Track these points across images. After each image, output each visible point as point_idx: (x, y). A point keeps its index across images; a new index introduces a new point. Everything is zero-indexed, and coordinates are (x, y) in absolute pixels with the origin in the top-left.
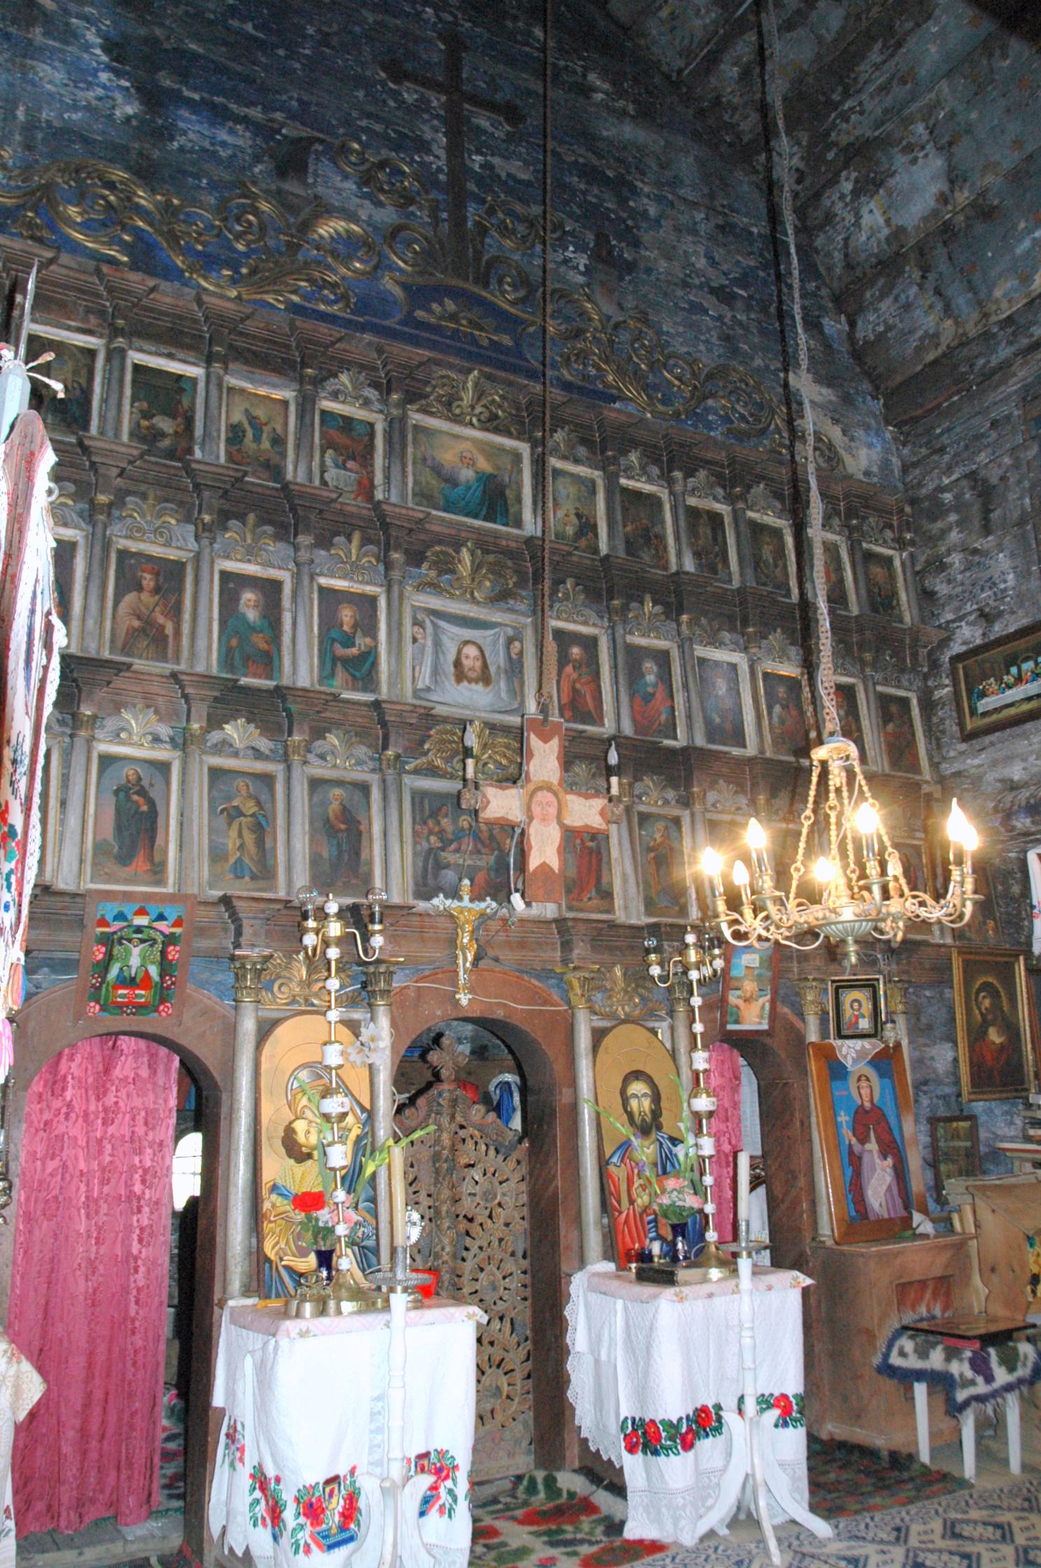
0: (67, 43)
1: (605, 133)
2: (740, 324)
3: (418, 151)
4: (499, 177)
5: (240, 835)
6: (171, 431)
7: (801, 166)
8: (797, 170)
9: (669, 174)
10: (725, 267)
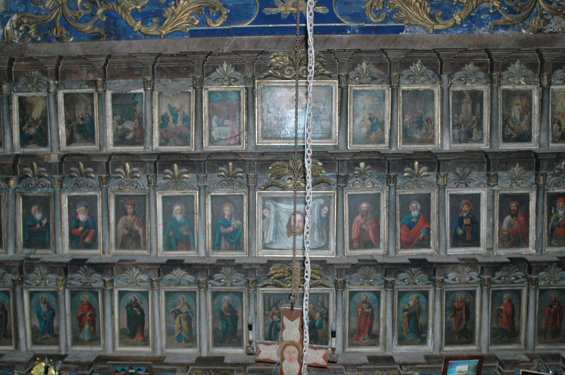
5: (180, 322)
6: (132, 128)
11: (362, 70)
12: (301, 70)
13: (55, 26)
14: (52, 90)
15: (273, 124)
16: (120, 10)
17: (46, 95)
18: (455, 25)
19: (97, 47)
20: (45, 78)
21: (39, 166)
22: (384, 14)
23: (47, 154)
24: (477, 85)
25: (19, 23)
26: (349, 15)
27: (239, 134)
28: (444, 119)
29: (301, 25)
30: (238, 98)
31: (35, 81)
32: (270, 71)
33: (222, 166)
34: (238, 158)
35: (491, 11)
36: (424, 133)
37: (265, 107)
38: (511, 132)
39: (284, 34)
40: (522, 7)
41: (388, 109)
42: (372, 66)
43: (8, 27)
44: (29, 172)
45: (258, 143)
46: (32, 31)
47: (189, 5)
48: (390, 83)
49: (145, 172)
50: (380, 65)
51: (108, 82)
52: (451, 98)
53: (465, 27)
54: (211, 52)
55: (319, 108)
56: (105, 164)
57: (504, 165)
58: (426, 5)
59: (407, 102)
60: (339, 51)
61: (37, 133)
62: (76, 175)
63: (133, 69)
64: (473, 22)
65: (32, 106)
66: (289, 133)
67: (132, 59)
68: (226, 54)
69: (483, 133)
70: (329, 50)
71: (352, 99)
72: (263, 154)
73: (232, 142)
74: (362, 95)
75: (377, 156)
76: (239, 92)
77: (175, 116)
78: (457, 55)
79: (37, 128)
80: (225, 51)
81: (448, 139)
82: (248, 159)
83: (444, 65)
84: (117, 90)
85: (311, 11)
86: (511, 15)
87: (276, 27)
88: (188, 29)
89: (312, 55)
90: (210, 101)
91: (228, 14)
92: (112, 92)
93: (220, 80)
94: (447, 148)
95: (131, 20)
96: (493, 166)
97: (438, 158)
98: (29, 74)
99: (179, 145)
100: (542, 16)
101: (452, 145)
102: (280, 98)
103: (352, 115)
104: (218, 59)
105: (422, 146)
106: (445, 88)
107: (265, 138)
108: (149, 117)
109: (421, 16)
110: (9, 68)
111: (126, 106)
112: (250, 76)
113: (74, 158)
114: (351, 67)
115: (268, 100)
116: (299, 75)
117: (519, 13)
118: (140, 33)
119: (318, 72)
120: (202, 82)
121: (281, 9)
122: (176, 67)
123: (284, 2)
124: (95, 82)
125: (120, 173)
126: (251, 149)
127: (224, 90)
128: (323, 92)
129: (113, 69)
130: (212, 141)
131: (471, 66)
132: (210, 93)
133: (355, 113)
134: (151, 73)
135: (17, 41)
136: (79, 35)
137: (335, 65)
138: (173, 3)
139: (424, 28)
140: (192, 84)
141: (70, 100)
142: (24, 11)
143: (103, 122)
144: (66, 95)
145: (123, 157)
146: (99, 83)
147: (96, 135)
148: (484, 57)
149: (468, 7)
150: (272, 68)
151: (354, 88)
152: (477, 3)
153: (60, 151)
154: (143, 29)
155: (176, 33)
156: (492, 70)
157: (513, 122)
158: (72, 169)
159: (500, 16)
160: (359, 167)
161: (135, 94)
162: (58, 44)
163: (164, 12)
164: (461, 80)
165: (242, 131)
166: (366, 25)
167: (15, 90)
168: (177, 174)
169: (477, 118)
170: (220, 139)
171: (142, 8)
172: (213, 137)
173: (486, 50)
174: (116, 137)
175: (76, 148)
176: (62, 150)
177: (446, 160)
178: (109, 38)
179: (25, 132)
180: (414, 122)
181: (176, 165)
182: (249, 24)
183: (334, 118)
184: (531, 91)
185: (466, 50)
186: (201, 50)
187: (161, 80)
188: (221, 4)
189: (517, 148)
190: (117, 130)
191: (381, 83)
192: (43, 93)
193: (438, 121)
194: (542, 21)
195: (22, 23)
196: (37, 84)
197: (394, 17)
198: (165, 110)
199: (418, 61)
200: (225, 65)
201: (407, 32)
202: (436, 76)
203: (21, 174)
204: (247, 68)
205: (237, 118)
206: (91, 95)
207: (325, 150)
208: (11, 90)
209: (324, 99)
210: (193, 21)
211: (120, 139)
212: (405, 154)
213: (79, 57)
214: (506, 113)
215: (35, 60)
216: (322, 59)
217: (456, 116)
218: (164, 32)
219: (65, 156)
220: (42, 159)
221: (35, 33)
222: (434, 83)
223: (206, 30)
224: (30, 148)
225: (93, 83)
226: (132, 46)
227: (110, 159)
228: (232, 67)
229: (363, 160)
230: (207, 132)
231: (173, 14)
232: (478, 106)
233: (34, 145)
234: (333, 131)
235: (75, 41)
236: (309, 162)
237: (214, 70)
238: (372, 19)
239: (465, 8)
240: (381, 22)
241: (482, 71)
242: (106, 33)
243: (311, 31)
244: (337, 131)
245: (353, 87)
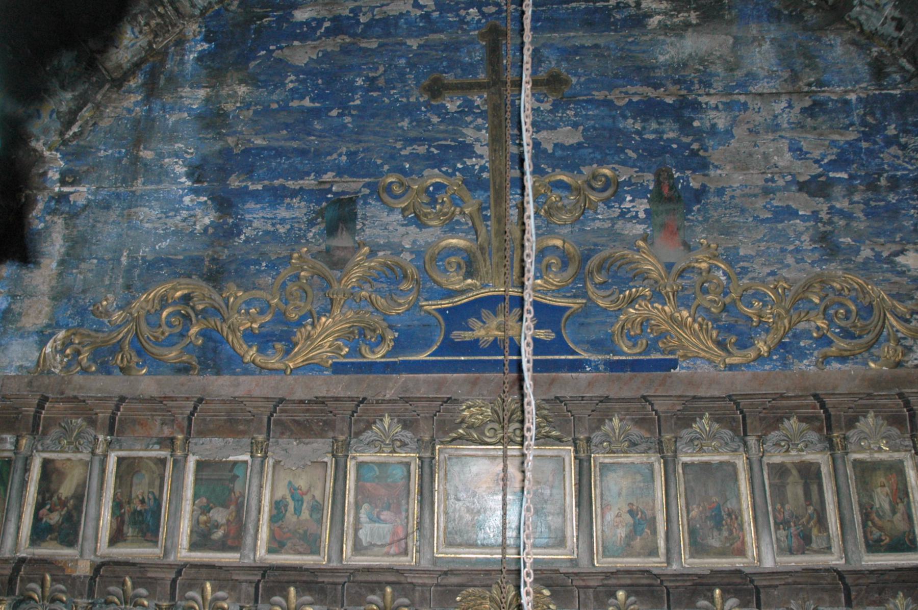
0: (160, 182)
1: (662, 59)
2: (841, 213)
3: (460, 159)
4: (545, 151)
6: (224, 521)
7: (897, 14)
8: (893, 19)
9: (739, 74)
10: (816, 154)
11: (613, 430)
12: (511, 430)
13: (122, 349)
14: (99, 451)
15: (464, 521)
16: (225, 329)
17: (88, 459)
18: (759, 356)
19: (182, 385)
20: (91, 431)
21: (54, 580)
22: (644, 342)
23: (72, 561)
24: (808, 453)
25: (66, 343)
26: (588, 342)
27: (406, 537)
28: (759, 513)
29: (510, 358)
30: (405, 473)
31: (75, 434)
32: (461, 431)
33: (373, 592)
34: (402, 579)
35: (815, 335)
36: (726, 538)
37: (451, 491)
38: (878, 534)
39: (484, 372)
40: (863, 328)
41: (660, 495)
42: (629, 423)
43: (48, 349)
44: (34, 591)
45: (438, 553)
46: (84, 357)
47: (334, 324)
48: (661, 451)
49: (238, 600)
50: (642, 422)
51: (193, 441)
52: (766, 476)
53: (776, 360)
54: (364, 399)
55: (542, 494)
56: (169, 582)
57: (877, 595)
58: (710, 326)
59: (692, 484)
60: (573, 398)
61: (62, 523)
62: (116, 600)
63: (237, 422)
64: (787, 352)
65: (62, 475)
66: (492, 535)
67: (236, 406)
68: (389, 401)
69: (829, 535)
70: (557, 398)
71: (598, 478)
72: (446, 573)
73: (393, 550)
74: (615, 471)
75: (647, 578)
76: (408, 465)
77: (299, 501)
78: (768, 405)
79: (63, 513)
80: (388, 397)
81: (770, 547)
82: (420, 581)
83: (748, 421)
84: (207, 456)
85: (529, 339)
86: (848, 341)
87: (472, 361)
88: (330, 362)
89: (531, 409)
90: (358, 478)
91: (395, 340)
92: (197, 458)
93: (377, 443)
94: (769, 563)
95: (241, 345)
96: (855, 598)
97: (756, 583)
98: (67, 423)
99: (300, 553)
100: (898, 341)
101: (778, 559)
102: (477, 475)
103: (598, 505)
104: (375, 410)
105: (724, 560)
106: (755, 458)
107: (450, 544)
108: (254, 503)
109: (703, 344)
110: (37, 412)
111: (218, 483)
112: (427, 438)
113: (117, 568)
114: (594, 426)
115: (457, 479)
116: (509, 437)
117: (860, 337)
118: (253, 365)
119: (540, 432)
120: (347, 446)
121: (480, 333)
122: (307, 420)
123: (484, 323)
124: (172, 440)
125: (193, 599)
126: (425, 564)
127: (382, 460)
128: (549, 467)
129: (205, 420)
130: (358, 548)
131: (794, 421)
132: (360, 465)
133: (604, 502)
134: (265, 430)
135: (57, 371)
136: (157, 365)
137: (567, 421)
138: (310, 320)
139: (710, 361)
140: (330, 449)
141: (127, 468)
142: (78, 325)
143: (176, 507)
144: (120, 460)
145: (203, 570)
146: (178, 443)
147: (161, 529)
148: (814, 407)
149: (777, 329)
150: (464, 426)
151: (601, 460)
152: (790, 323)
153: (96, 556)
154: (258, 359)
155: (312, 367)
156: (829, 428)
157: (879, 516)
158: (112, 589)
159: (830, 343)
160: (616, 599)
161: (235, 463)
162: (121, 377)
163: (295, 334)
164: (780, 445)
165: (410, 531)
166: (616, 358)
167: (40, 448)
168: (293, 606)
169: (815, 510)
170: (372, 545)
171: (261, 326)
172: (361, 540)
173: (816, 396)
174: (195, 535)
175: (123, 551)
176: (98, 553)
177: (770, 586)
178: (202, 372)
179: (41, 519)
180: (707, 517)
181: (292, 590)
182: (429, 356)
183: (568, 510)
184: (901, 462)
185: (782, 397)
186: (349, 394)
187: (280, 441)
188: (385, 324)
189: (893, 562)
190: (198, 522)
191: (645, 452)
192: (85, 456)
193: (748, 516)
194: (900, 349)
195: (72, 343)
196: (76, 439)
197: (661, 345)
198: (282, 491)
199: (704, 414)
200: (387, 420)
201: (682, 368)
202: (737, 439)
203: (21, 594)
204: (423, 425)
205: (404, 507)
206: (162, 462)
207: (554, 567)
208: (33, 448)
209: (551, 479)
210: (340, 348)
211: (201, 540)
212: (696, 575)
213: (152, 399)
214: (865, 500)
215: (81, 401)
216: (546, 412)
217: (778, 506)
218: (291, 365)
219: (103, 564)
220: (63, 569)
221: (88, 360)
222: (735, 451)
223: (360, 363)
224: (46, 548)
225: (168, 442)
226: (238, 385)
227: (179, 573)
228: (399, 422)
229: (621, 587)
230: (351, 531)
231: (309, 337)
232: (814, 488)
233: (54, 543)
234: (568, 534)
235: (149, 373)
236: (528, 594)
237: (368, 426)
238: (625, 349)
239: (772, 331)
240: (640, 354)
241: (814, 430)
242: (199, 363)
243: (528, 370)
244: (575, 534)
245: (600, 458)
